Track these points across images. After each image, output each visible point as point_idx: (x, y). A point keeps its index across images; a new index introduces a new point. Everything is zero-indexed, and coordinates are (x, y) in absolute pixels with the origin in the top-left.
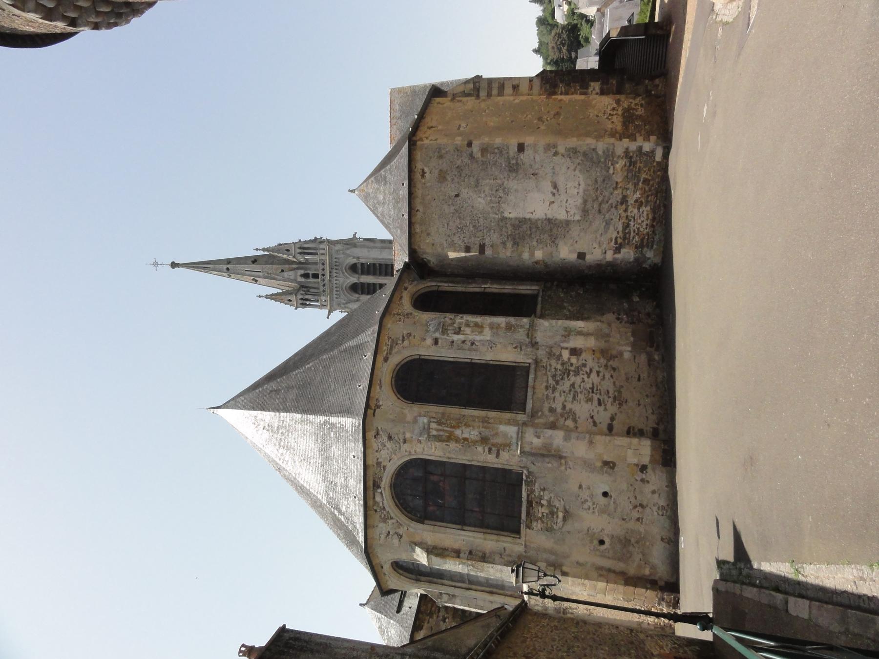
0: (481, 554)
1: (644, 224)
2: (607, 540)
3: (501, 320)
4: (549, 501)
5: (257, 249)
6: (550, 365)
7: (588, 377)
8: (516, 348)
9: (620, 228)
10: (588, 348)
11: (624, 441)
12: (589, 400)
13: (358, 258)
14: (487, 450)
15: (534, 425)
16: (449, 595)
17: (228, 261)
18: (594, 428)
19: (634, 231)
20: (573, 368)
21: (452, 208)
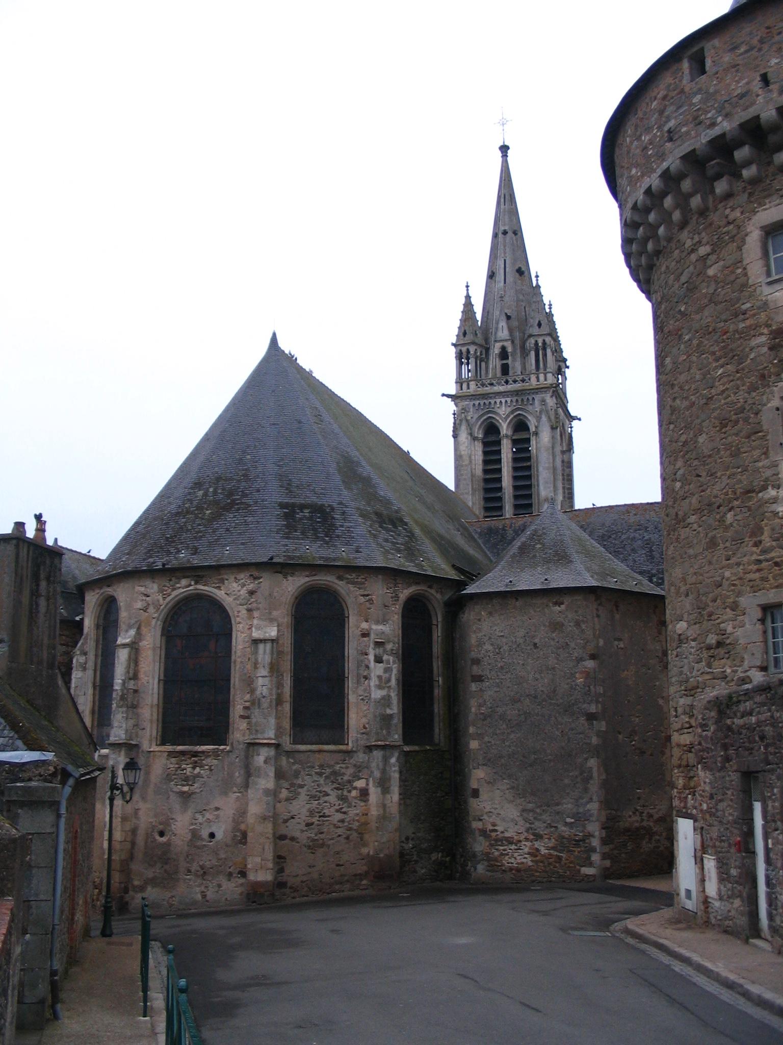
0: (135, 703)
1: (512, 860)
2: (164, 839)
3: (395, 709)
4: (199, 775)
5: (537, 276)
6: (347, 768)
7: (337, 811)
8: (365, 727)
9: (507, 835)
10: (369, 809)
11: (269, 855)
12: (311, 813)
13: (536, 434)
14: (247, 704)
15: (277, 757)
16: (85, 663)
17: (517, 232)
18: (281, 821)
19: (504, 850)
20: (345, 793)
21: (521, 641)
